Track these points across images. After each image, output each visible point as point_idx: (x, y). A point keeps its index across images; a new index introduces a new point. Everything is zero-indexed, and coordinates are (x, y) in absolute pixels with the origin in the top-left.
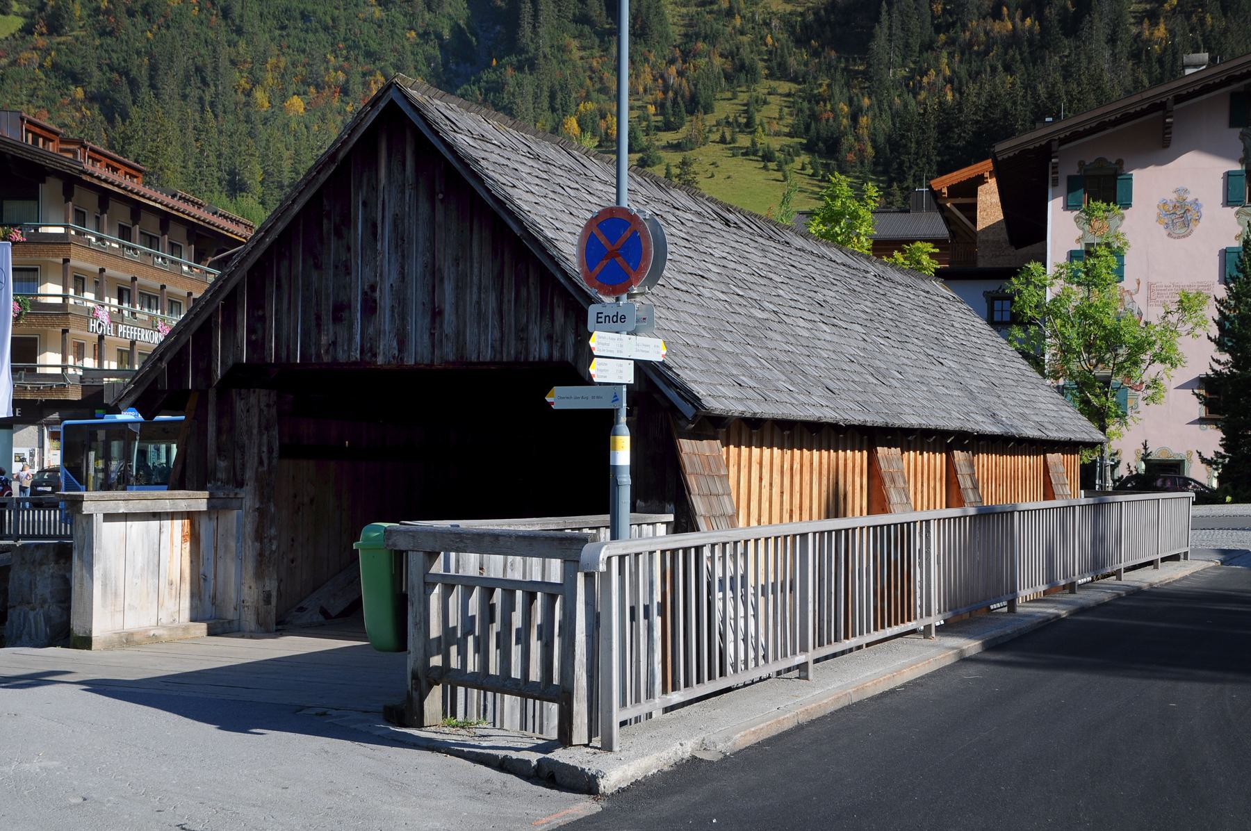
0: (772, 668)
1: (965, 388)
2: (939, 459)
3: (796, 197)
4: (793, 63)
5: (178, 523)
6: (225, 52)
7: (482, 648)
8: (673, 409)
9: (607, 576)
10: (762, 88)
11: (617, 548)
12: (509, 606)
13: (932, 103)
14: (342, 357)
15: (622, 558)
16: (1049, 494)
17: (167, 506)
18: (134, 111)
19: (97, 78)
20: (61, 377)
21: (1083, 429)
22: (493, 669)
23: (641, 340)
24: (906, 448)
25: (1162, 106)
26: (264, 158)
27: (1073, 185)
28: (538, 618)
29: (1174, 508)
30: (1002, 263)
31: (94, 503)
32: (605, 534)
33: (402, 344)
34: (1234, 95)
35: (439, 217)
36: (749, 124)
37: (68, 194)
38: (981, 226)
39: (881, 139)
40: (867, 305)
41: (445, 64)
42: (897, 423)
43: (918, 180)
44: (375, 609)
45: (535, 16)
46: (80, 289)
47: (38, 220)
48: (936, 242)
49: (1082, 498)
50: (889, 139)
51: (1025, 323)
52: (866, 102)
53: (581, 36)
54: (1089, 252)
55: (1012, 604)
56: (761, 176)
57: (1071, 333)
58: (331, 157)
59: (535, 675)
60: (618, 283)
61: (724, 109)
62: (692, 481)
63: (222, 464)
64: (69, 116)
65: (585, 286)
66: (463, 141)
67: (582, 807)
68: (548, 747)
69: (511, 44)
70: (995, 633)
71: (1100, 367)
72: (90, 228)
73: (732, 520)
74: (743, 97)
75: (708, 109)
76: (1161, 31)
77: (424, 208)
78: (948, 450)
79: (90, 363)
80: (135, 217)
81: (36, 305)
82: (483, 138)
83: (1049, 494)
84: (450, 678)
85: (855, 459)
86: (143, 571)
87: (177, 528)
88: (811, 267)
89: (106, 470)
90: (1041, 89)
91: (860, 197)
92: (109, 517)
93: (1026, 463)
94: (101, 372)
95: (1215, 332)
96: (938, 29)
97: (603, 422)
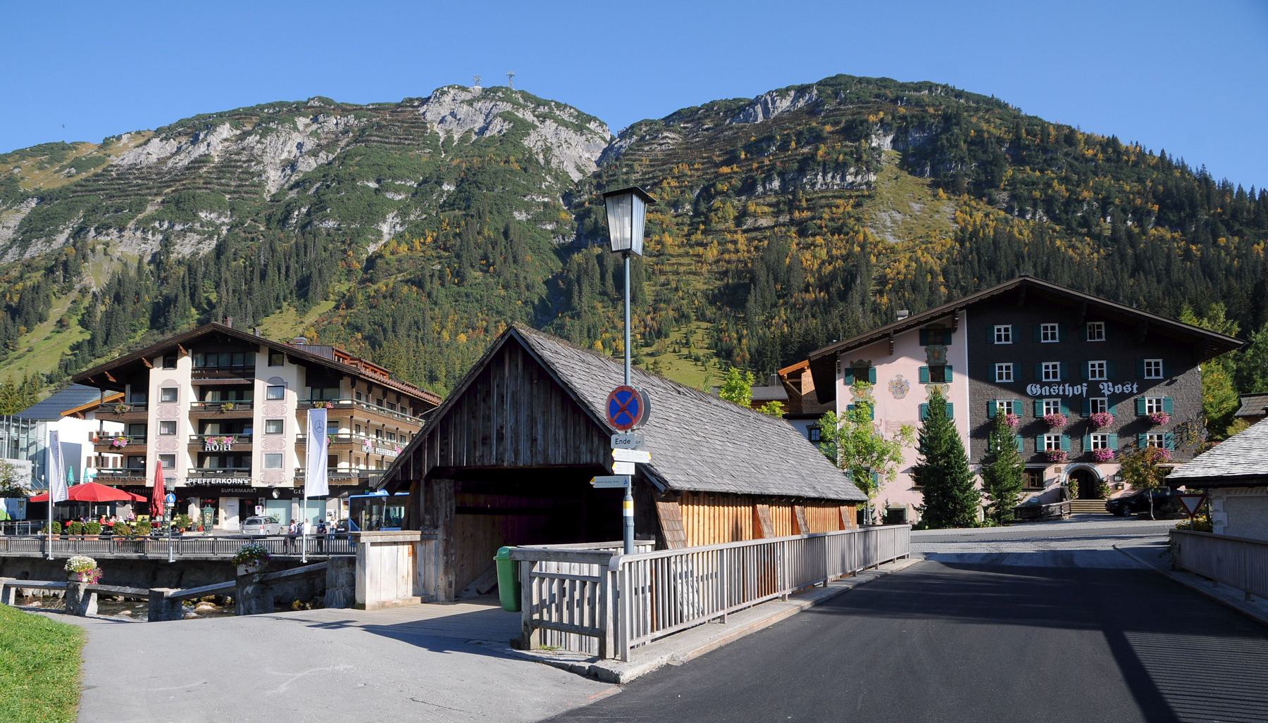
0: (706, 619)
1: (799, 474)
2: (788, 510)
3: (712, 379)
4: (708, 313)
5: (406, 547)
6: (428, 314)
7: (559, 610)
8: (654, 487)
9: (622, 573)
10: (693, 325)
11: (627, 559)
12: (573, 589)
13: (778, 333)
14: (486, 463)
15: (630, 563)
16: (842, 527)
17: (400, 538)
18: (385, 344)
19: (368, 328)
20: (349, 474)
21: (857, 494)
22: (566, 620)
23: (638, 452)
24: (771, 505)
25: (888, 335)
26: (447, 364)
27: (848, 373)
28: (587, 595)
29: (901, 533)
30: (814, 411)
31: (366, 537)
32: (621, 551)
33: (517, 454)
34: (921, 330)
35: (535, 392)
36: (687, 343)
37: (353, 385)
38: (803, 393)
39: (753, 350)
40: (749, 433)
41: (536, 316)
42: (767, 492)
43: (772, 370)
44: (505, 590)
45: (580, 292)
46: (358, 430)
47: (338, 397)
48: (782, 401)
49: (858, 529)
50: (757, 351)
51: (827, 442)
52: (745, 332)
53: (603, 301)
54: (857, 406)
55: (825, 582)
56: (694, 369)
57: (850, 446)
58: (481, 363)
59: (586, 623)
60: (626, 424)
61: (675, 336)
62: (664, 523)
63: (428, 517)
64: (355, 347)
65: (610, 426)
66: (547, 354)
67: (611, 690)
68: (593, 660)
69: (568, 306)
70: (817, 598)
71: (864, 463)
72: (363, 400)
73: (685, 543)
74: (684, 330)
75: (666, 336)
76: (885, 300)
77: (527, 387)
78: (792, 505)
79: (362, 467)
80: (385, 396)
81: (337, 439)
82: (556, 352)
83: (842, 527)
84: (544, 625)
85: (746, 511)
86: (390, 570)
87: (406, 549)
88: (722, 415)
89: (370, 520)
90: (830, 326)
91: (744, 379)
92: (373, 544)
93: (831, 511)
94: (368, 471)
95: (918, 445)
96: (779, 297)
97: (621, 493)
